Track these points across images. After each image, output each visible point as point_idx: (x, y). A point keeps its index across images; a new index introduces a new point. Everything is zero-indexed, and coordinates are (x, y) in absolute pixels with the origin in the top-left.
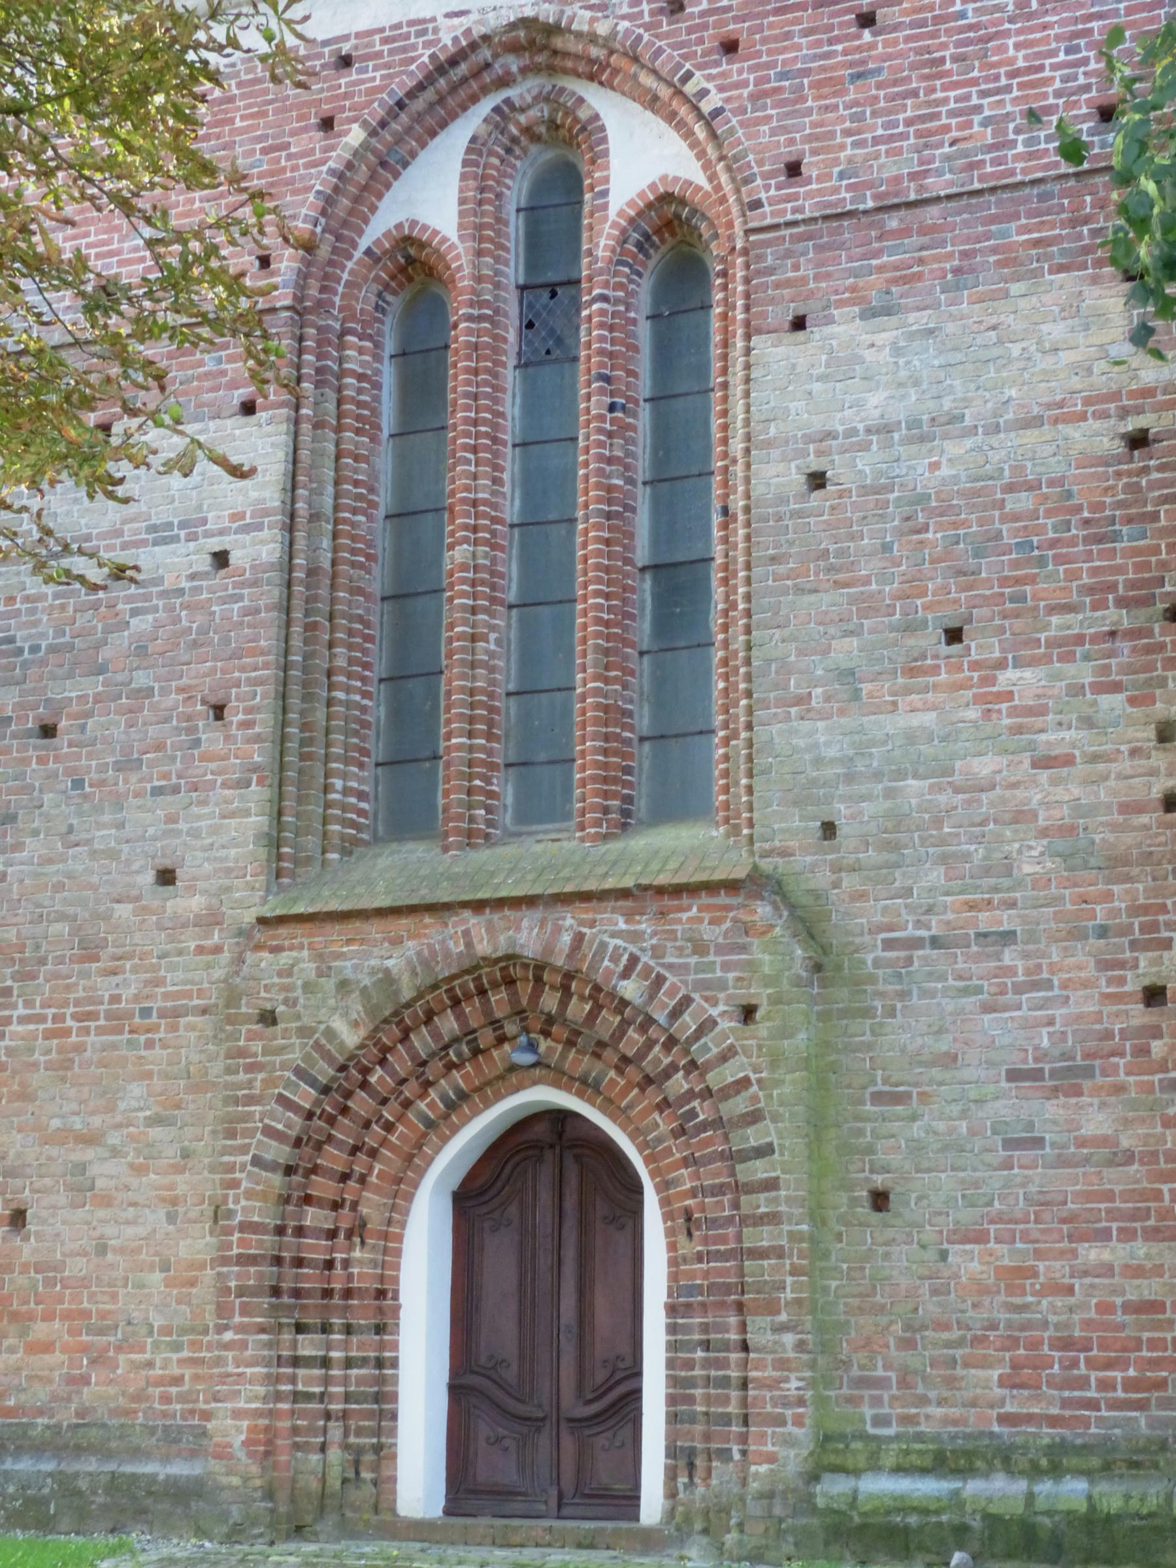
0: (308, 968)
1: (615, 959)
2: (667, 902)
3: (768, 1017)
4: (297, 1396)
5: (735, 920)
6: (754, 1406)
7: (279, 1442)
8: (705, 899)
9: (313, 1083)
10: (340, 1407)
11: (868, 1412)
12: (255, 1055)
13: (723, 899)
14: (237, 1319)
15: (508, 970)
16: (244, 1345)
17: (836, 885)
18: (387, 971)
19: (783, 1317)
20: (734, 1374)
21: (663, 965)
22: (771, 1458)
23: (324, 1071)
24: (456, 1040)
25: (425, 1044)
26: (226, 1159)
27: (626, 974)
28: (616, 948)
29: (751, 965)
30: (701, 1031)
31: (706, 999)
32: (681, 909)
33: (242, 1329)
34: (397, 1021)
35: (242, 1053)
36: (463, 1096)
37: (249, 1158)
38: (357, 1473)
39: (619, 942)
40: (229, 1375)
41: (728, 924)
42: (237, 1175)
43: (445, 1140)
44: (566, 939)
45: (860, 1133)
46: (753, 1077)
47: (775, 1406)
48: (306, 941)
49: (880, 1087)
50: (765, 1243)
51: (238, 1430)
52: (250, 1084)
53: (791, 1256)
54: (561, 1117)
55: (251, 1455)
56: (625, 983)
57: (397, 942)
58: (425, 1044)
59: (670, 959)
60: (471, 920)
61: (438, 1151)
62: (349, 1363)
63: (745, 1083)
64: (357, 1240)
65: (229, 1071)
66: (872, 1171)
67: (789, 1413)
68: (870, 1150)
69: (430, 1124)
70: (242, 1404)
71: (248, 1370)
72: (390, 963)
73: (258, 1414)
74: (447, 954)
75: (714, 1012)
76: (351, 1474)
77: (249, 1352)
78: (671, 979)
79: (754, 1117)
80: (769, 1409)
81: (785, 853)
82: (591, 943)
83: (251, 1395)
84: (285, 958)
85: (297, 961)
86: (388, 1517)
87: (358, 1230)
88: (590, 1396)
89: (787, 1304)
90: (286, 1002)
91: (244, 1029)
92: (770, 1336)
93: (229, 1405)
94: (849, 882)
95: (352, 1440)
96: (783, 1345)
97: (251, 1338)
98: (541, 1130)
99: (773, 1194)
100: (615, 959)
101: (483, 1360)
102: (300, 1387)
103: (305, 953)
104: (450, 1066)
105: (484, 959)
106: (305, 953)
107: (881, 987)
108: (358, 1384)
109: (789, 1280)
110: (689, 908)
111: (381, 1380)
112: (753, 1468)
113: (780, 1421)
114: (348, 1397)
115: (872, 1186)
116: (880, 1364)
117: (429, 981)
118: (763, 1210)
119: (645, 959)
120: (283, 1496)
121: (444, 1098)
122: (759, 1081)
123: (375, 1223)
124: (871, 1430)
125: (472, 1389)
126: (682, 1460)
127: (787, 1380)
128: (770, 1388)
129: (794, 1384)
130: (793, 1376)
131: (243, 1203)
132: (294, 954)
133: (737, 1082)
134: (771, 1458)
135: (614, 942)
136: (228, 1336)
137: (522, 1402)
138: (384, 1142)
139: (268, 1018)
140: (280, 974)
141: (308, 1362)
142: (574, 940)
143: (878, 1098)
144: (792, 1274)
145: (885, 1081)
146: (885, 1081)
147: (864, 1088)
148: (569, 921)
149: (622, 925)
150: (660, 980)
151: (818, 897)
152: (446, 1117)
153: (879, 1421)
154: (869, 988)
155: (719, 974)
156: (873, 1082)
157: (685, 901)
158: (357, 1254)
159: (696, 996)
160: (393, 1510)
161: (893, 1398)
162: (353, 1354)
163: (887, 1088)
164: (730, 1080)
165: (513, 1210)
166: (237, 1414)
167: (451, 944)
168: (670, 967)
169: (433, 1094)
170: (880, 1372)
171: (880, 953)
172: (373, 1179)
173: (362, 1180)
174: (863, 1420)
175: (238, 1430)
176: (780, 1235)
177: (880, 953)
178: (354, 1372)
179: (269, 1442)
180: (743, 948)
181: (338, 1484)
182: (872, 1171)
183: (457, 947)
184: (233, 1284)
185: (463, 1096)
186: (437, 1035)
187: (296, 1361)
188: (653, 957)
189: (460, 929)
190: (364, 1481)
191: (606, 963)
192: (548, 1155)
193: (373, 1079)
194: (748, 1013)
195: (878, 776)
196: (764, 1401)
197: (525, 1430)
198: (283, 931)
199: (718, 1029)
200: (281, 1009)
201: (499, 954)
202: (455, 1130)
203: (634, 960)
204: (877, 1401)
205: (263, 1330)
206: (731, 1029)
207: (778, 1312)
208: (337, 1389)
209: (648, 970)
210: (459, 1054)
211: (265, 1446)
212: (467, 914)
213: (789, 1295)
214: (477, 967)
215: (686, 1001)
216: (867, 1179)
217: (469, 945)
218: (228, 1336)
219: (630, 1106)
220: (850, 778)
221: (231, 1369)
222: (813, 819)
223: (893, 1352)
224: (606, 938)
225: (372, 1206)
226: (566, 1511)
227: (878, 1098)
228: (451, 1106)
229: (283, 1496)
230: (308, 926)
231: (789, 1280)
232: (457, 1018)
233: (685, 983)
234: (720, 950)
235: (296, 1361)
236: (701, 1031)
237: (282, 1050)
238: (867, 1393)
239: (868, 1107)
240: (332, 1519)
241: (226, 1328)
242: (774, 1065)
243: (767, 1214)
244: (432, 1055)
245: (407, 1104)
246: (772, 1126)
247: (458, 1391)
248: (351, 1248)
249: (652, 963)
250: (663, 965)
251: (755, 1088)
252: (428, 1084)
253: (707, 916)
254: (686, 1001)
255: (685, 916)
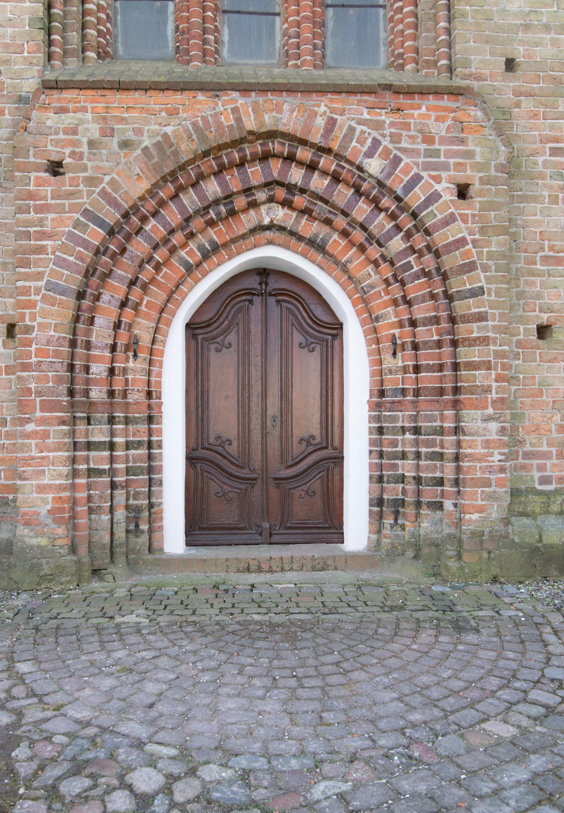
0: (94, 130)
1: (361, 142)
2: (402, 100)
3: (481, 193)
4: (91, 472)
5: (454, 119)
6: (468, 473)
7: (79, 509)
8: (432, 100)
9: (101, 223)
10: (124, 479)
11: (537, 475)
12: (45, 198)
13: (446, 102)
14: (38, 414)
15: (268, 144)
16: (46, 435)
17: (518, 105)
18: (165, 135)
19: (490, 411)
20: (410, 449)
21: (399, 149)
22: (481, 510)
23: (112, 216)
24: (217, 202)
25: (193, 202)
26: (19, 284)
27: (370, 154)
28: (363, 132)
29: (470, 155)
30: (429, 201)
31: (433, 178)
32: (413, 107)
33: (43, 421)
34: (177, 177)
35: (31, 196)
36: (216, 248)
37: (43, 283)
38: (137, 526)
39: (365, 128)
40: (33, 458)
41: (449, 122)
42: (33, 297)
43: (197, 281)
44: (320, 122)
45: (533, 283)
46: (469, 238)
47: (484, 472)
48: (89, 106)
49: (547, 253)
50: (476, 359)
51: (44, 501)
52: (41, 223)
53: (495, 369)
54: (263, 272)
55: (55, 521)
56: (367, 160)
57: (173, 112)
58: (193, 202)
59: (404, 145)
60: (240, 101)
61: (191, 289)
62: (128, 446)
63: (462, 242)
64: (131, 354)
65: (20, 210)
66: (541, 311)
67: (493, 477)
68: (539, 296)
69: (189, 269)
70: (46, 481)
71: (51, 454)
72: (169, 130)
73: (61, 488)
74: (219, 126)
75: (438, 187)
76: (132, 527)
77: (51, 440)
78: (406, 160)
79: (470, 267)
80: (479, 475)
81: (479, 78)
82: (341, 127)
83: (55, 474)
84: (68, 119)
85: (81, 122)
86: (157, 556)
87: (133, 347)
88: (290, 463)
89: (493, 402)
90: (73, 154)
91: (33, 175)
92: (479, 424)
93: (34, 482)
94: (527, 104)
95: (131, 502)
96: (489, 431)
97: (52, 429)
98: (253, 282)
99: (484, 323)
100: (361, 142)
101: (212, 440)
102: (92, 466)
103: (89, 116)
104: (211, 223)
105: (251, 133)
106: (89, 116)
107: (548, 181)
108: (134, 461)
109: (494, 385)
110: (419, 108)
111: (150, 457)
112: (467, 516)
113: (487, 483)
114: (128, 471)
115: (539, 322)
116: (545, 443)
117: (204, 148)
118: (475, 335)
119: (386, 142)
120: (83, 550)
121: (201, 248)
122: (474, 242)
123: (145, 339)
124: (539, 487)
125: (198, 459)
126: (381, 507)
127: (492, 455)
128: (480, 460)
129: (497, 457)
130: (496, 452)
131: (39, 320)
132: (79, 115)
133: (457, 241)
134: (481, 510)
135: (359, 128)
136: (30, 427)
137: (241, 467)
138: (153, 280)
139: (55, 168)
140: (66, 132)
141: (97, 446)
142: (327, 123)
143: (545, 260)
144: (496, 381)
145: (551, 248)
146: (551, 248)
147: (536, 253)
148: (323, 109)
149: (366, 116)
150: (397, 161)
151: (504, 113)
152: (199, 264)
153: (545, 480)
154: (540, 182)
155: (442, 159)
156: (542, 249)
157: (417, 100)
158: (131, 364)
159: (425, 174)
160: (161, 550)
161: (554, 465)
162: (131, 439)
163: (551, 254)
164: (451, 239)
165: (232, 338)
166: (41, 489)
167: (223, 119)
168: (404, 151)
169: (192, 245)
170: (545, 448)
171: (547, 157)
172: (143, 308)
173: (136, 307)
174: (533, 481)
175: (44, 501)
176: (488, 355)
177: (547, 157)
178: (132, 452)
179: (72, 509)
180: (462, 141)
181: (123, 535)
182: (541, 311)
183: (228, 120)
184: (33, 386)
185: (216, 248)
186: (202, 196)
187: (89, 446)
188: (392, 142)
189: (229, 107)
190: (142, 532)
191: (354, 143)
192: (257, 300)
193: (148, 228)
194: (463, 192)
195: (547, 28)
196: (474, 469)
197: (243, 487)
198: (68, 95)
199: (442, 200)
200: (67, 160)
201: (264, 130)
202: (205, 274)
203: (376, 143)
204: (541, 468)
205: (63, 423)
206: (451, 201)
207: (487, 408)
208: (121, 466)
209: (387, 151)
210: (218, 214)
211: (67, 514)
212: (235, 94)
213: (494, 396)
214: (242, 141)
215: (417, 178)
216: (537, 316)
217: (238, 120)
218: (30, 427)
219: (349, 261)
220: (527, 27)
221: (34, 453)
222: (502, 55)
223: (554, 435)
224: (353, 124)
225: (143, 330)
226: (275, 538)
227: (545, 260)
228: (206, 256)
229: (83, 550)
230: (90, 92)
231: (494, 385)
232: (220, 185)
233: (417, 164)
234: (443, 141)
235: (89, 446)
236: (429, 201)
237: (70, 195)
238: (535, 462)
239: (538, 266)
240: (121, 561)
241: (29, 420)
242: (483, 231)
243: (479, 338)
244: (197, 212)
245: (173, 250)
246: (482, 275)
247: (191, 460)
248: (127, 360)
249: (390, 146)
250: (399, 149)
251: (470, 246)
252: (192, 235)
253: (433, 115)
254: (417, 178)
255: (416, 113)
